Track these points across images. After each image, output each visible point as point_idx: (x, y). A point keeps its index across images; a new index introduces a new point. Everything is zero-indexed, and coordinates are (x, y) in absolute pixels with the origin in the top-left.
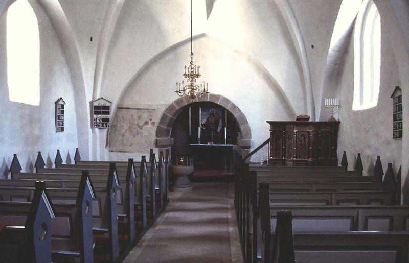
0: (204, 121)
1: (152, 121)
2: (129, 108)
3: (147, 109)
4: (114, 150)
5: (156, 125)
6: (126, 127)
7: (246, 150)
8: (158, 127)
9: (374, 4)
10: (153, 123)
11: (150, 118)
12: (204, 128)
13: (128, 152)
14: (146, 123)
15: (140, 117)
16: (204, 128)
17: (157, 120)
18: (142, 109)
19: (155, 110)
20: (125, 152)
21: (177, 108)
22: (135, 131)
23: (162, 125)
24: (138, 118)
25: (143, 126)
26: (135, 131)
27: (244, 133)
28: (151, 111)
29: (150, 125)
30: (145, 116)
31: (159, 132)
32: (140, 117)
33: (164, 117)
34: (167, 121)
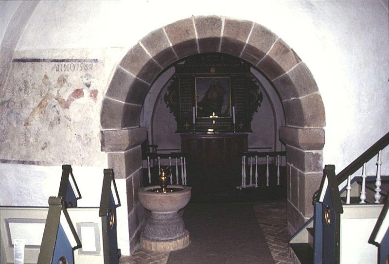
0: (202, 97)
1: (91, 88)
2: (38, 60)
3: (80, 61)
4: (9, 158)
5: (101, 97)
6: (33, 104)
7: (314, 152)
8: (106, 103)
9: (45, 224)
10: (94, 94)
11: (85, 81)
12: (201, 108)
13: (38, 163)
14: (78, 93)
15: (62, 81)
16: (201, 108)
17: (102, 81)
18: (67, 61)
19: (96, 61)
20: (33, 163)
21: (150, 54)
22: (52, 116)
23: (125, 67)
24: (59, 81)
25: (70, 100)
26: (52, 116)
27: (308, 113)
28: (86, 64)
29: (86, 98)
30: (74, 78)
31: (107, 115)
32: (64, 80)
33: (119, 76)
34: (126, 87)
